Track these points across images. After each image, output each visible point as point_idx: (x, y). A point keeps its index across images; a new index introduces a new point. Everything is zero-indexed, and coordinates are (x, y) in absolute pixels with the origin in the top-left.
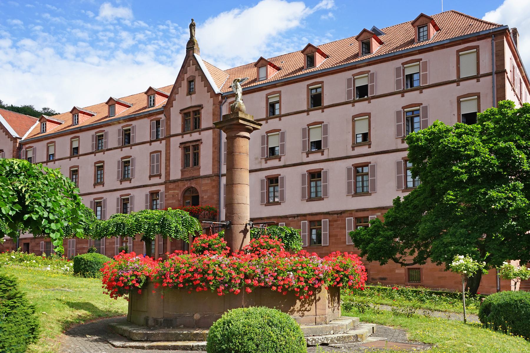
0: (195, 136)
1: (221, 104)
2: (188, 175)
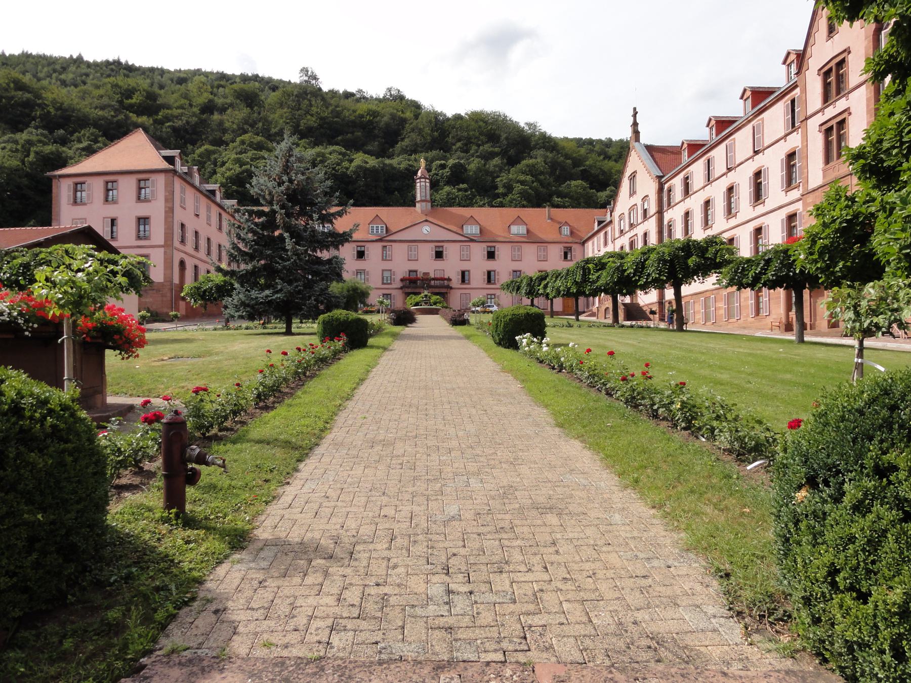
0: (841, 105)
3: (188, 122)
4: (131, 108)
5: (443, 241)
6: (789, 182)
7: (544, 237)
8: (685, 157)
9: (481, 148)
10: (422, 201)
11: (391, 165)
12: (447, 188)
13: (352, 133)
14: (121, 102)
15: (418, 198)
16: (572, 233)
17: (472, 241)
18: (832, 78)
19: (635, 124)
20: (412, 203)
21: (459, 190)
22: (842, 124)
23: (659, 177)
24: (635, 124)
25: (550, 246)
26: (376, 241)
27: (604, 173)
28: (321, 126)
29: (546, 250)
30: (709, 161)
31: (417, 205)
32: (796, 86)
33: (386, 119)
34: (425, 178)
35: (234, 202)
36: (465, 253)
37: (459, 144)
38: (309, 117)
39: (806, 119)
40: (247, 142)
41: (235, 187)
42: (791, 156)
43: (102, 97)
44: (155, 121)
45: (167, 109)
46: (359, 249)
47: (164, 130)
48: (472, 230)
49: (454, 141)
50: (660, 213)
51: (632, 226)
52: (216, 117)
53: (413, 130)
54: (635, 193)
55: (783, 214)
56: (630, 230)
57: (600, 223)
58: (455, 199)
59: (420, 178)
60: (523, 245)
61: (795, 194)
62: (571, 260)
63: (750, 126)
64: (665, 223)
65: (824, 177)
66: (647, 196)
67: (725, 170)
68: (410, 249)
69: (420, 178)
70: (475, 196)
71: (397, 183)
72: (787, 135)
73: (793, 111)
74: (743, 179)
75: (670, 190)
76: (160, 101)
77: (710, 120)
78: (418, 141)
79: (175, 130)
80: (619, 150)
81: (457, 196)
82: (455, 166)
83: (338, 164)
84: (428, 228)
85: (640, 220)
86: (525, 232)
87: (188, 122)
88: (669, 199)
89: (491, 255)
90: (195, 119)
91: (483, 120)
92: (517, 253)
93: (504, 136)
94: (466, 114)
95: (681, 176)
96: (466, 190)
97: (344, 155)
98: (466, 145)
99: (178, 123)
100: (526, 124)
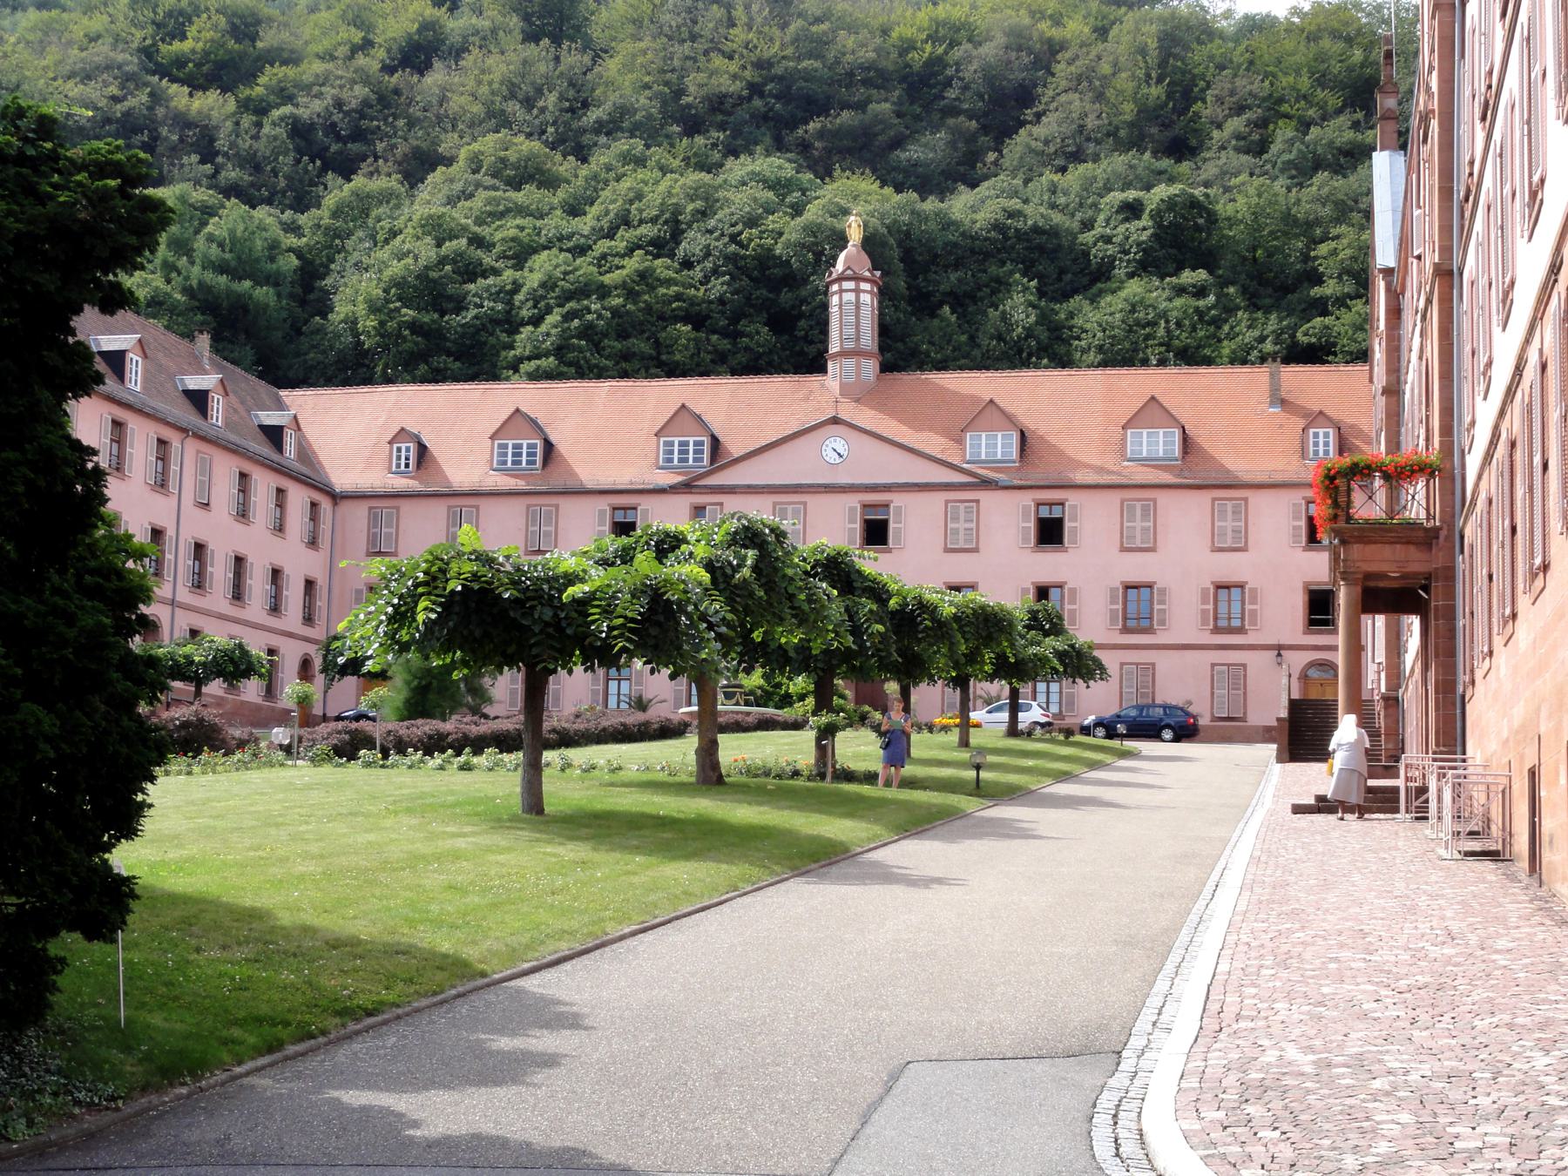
3: (339, 104)
4: (174, 70)
5: (887, 488)
7: (1239, 465)
9: (1314, 131)
10: (844, 354)
12: (1134, 288)
13: (861, 106)
14: (148, 53)
15: (834, 348)
17: (986, 484)
20: (815, 364)
21: (1180, 291)
25: (1257, 500)
28: (755, 89)
29: (1242, 511)
31: (831, 366)
33: (989, 51)
34: (857, 279)
35: (689, 327)
36: (962, 525)
37: (1236, 124)
38: (718, 61)
40: (488, 161)
41: (409, 313)
43: (94, 39)
44: (245, 105)
45: (285, 63)
46: (1045, 513)
47: (266, 129)
48: (995, 446)
49: (1220, 113)
52: (437, 77)
58: (1153, 324)
59: (840, 279)
60: (1163, 498)
68: (949, 516)
69: (840, 279)
70: (1230, 310)
76: (268, 39)
79: (299, 130)
81: (1164, 315)
82: (1170, 204)
83: (752, 222)
84: (840, 445)
86: (1177, 450)
87: (339, 104)
89: (1050, 532)
90: (360, 91)
92: (1139, 524)
96: (1200, 292)
97: (779, 186)
98: (1262, 124)
99: (310, 108)
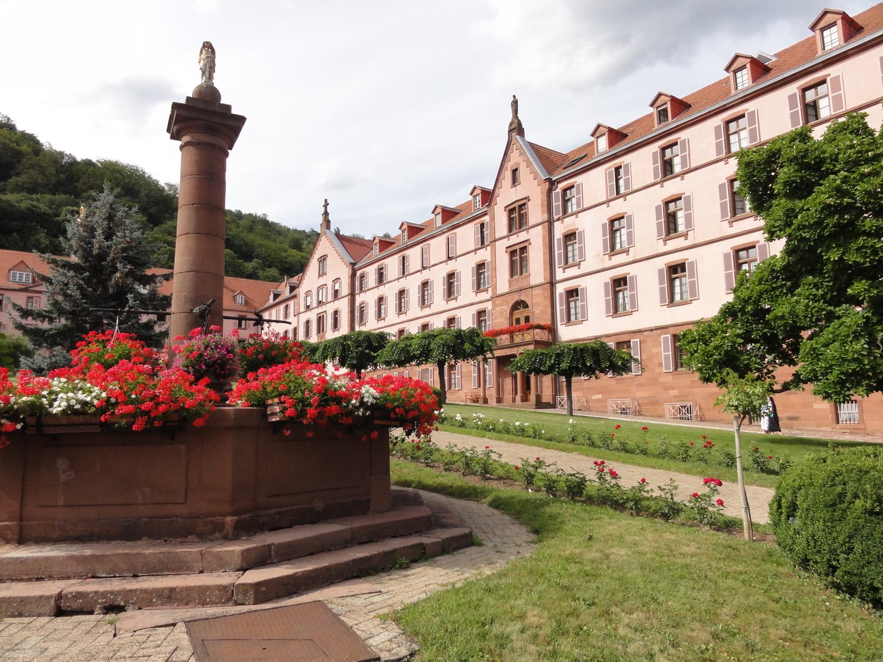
0: (523, 236)
1: (550, 191)
2: (516, 287)
6: (479, 286)
8: (376, 252)
11: (7, 201)
16: (246, 302)
18: (515, 215)
19: (326, 214)
22: (524, 249)
23: (353, 264)
24: (326, 214)
26: (20, 290)
27: (246, 244)
30: (404, 258)
32: (486, 214)
39: (495, 241)
42: (481, 266)
49: (84, 187)
50: (352, 295)
51: (320, 303)
53: (32, 166)
54: (324, 274)
55: (474, 309)
56: (317, 307)
57: (276, 296)
61: (484, 296)
62: (245, 329)
63: (444, 237)
64: (357, 304)
65: (510, 286)
66: (339, 279)
67: (420, 268)
71: (15, 223)
72: (476, 250)
73: (482, 232)
74: (437, 277)
75: (362, 277)
77: (403, 224)
78: (39, 180)
80: (250, 223)
85: (330, 299)
88: (361, 284)
91: (118, 171)
93: (144, 193)
94: (98, 161)
95: (376, 266)
100: (167, 184)
